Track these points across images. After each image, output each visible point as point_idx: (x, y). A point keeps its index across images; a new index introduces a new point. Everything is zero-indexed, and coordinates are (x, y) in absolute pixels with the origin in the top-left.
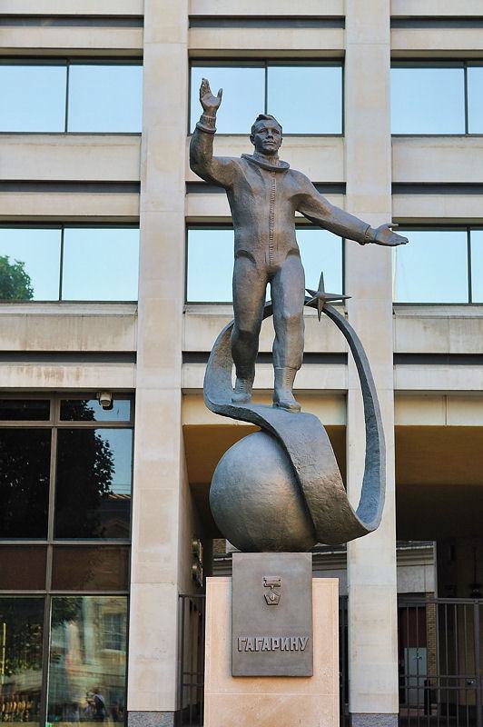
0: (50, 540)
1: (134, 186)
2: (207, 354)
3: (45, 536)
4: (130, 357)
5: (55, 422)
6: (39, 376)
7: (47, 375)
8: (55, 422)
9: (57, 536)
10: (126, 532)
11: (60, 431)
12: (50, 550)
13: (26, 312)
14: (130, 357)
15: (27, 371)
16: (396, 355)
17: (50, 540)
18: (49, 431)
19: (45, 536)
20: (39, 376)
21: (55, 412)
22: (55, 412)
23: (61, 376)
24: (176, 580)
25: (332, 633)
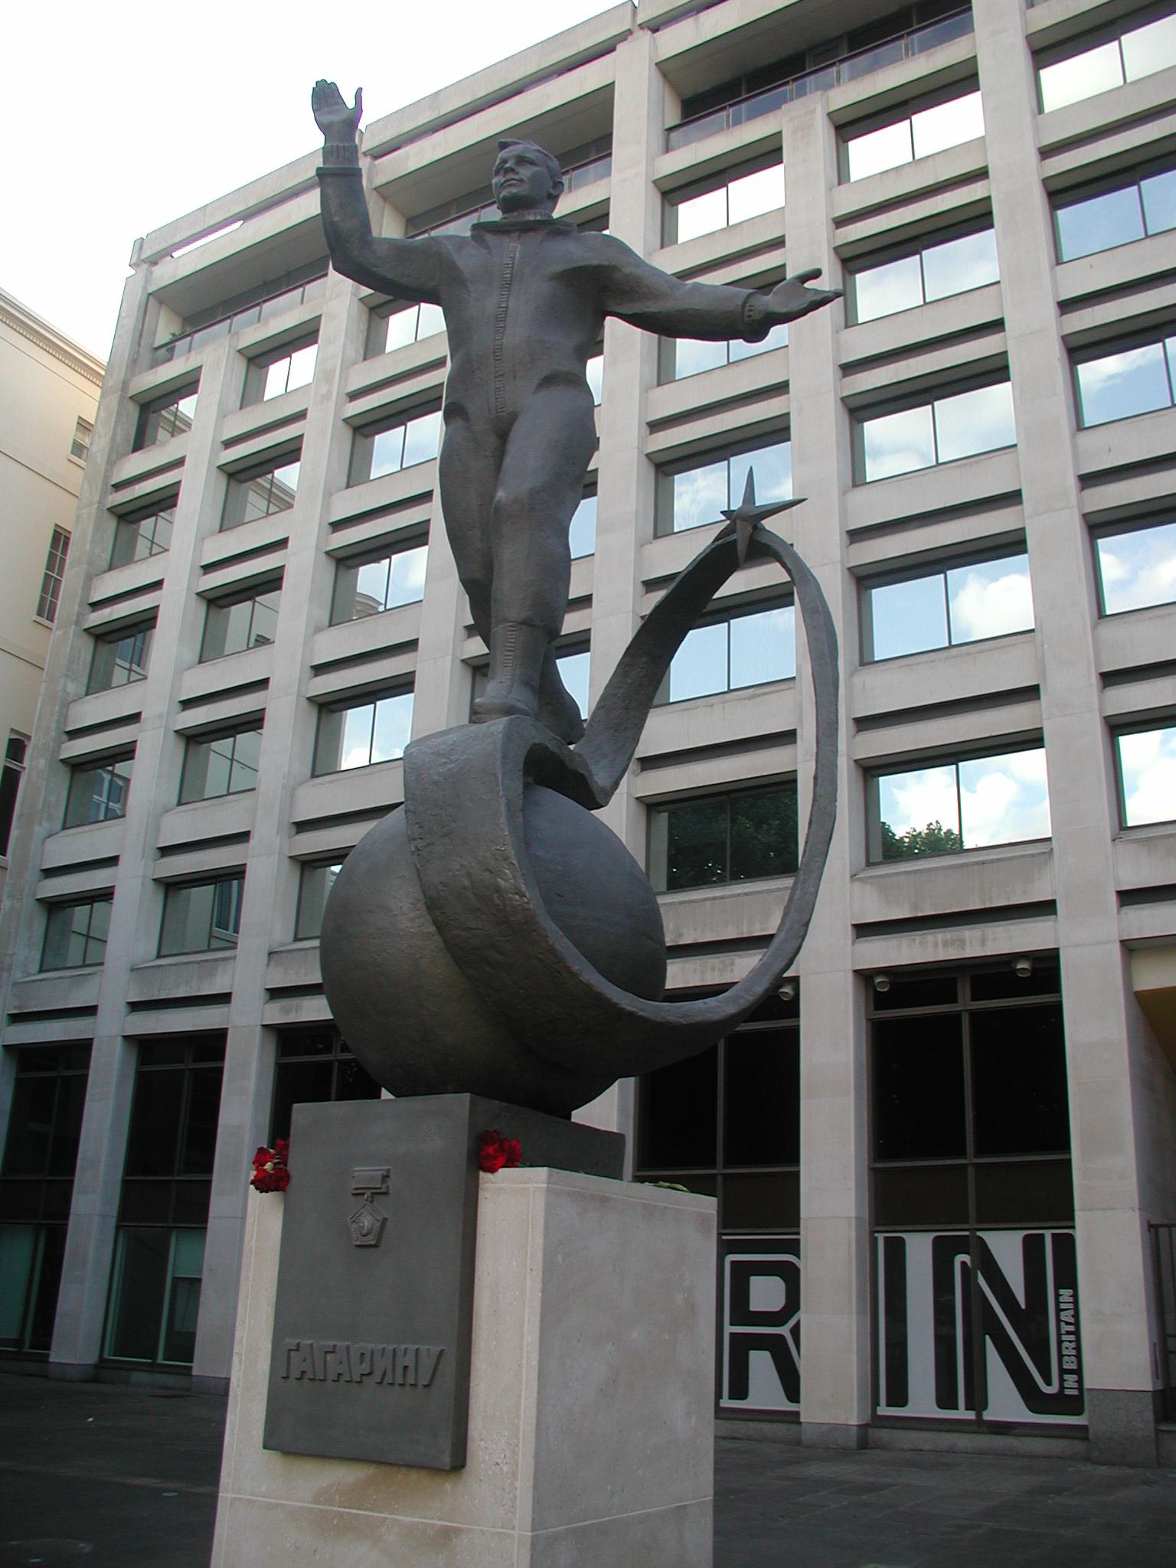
0: (971, 1159)
1: (1031, 693)
2: (769, 938)
3: (962, 1153)
4: (1047, 908)
5: (965, 1003)
6: (936, 945)
7: (945, 944)
8: (965, 1003)
9: (980, 1151)
10: (1066, 1146)
11: (974, 1015)
12: (971, 1171)
13: (710, 895)
14: (1047, 908)
15: (921, 943)
16: (1120, 893)
17: (971, 1159)
18: (956, 1017)
19: (962, 1153)
20: (936, 945)
21: (964, 991)
22: (964, 991)
23: (962, 943)
24: (1136, 1203)
25: (522, 1337)
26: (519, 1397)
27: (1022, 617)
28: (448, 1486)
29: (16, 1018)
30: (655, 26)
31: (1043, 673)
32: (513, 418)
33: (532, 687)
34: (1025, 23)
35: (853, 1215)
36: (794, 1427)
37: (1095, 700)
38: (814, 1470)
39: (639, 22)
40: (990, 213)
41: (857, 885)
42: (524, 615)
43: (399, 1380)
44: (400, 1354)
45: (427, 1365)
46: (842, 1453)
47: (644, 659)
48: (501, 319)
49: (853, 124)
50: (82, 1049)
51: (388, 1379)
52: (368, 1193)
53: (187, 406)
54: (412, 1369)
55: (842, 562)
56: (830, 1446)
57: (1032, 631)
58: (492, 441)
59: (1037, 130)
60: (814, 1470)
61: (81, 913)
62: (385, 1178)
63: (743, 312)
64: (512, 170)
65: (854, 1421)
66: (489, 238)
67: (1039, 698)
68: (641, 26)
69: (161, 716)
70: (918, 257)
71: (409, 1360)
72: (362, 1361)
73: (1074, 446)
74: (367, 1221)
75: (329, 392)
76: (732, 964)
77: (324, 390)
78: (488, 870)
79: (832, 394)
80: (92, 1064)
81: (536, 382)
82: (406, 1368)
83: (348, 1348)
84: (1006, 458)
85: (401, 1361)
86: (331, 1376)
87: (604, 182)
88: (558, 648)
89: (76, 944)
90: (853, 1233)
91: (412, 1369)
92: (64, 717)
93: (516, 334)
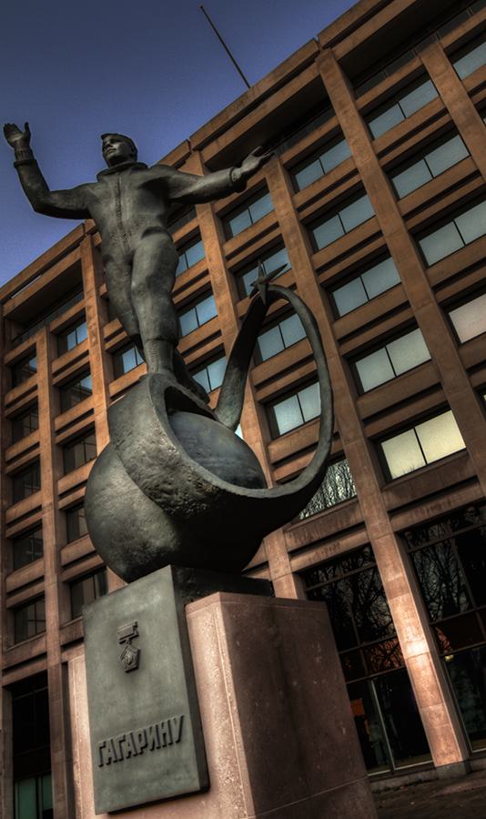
1: (437, 387)
20: (428, 511)
25: (225, 695)
26: (231, 731)
27: (424, 355)
28: (203, 802)
29: (7, 671)
30: (200, 148)
31: (440, 376)
32: (133, 253)
33: (169, 369)
34: (356, 106)
35: (428, 651)
36: (433, 772)
37: (468, 382)
38: (449, 790)
39: (192, 147)
40: (363, 187)
41: (384, 493)
42: (157, 335)
43: (162, 743)
44: (160, 727)
45: (175, 729)
46: (460, 779)
47: (236, 369)
48: (119, 211)
49: (292, 169)
50: (44, 674)
51: (157, 745)
52: (127, 639)
53: (33, 363)
54: (168, 734)
55: (339, 354)
56: (453, 776)
57: (430, 360)
58: (125, 268)
59: (373, 149)
60: (449, 790)
61: (30, 610)
62: (136, 627)
63: (231, 178)
64: (109, 146)
65: (461, 759)
66: (106, 178)
67: (442, 388)
68: (194, 150)
69: (51, 504)
70: (359, 279)
71: (166, 729)
72: (140, 740)
73: (426, 275)
74: (129, 655)
75: (96, 340)
76: (338, 544)
77: (94, 340)
78: (153, 442)
79: (315, 284)
80: (49, 682)
81: (141, 234)
82: (164, 735)
83: (131, 734)
84: (399, 288)
85: (161, 732)
86: (126, 755)
87: (195, 220)
88: (190, 370)
89: (31, 626)
90: (431, 660)
91: (168, 734)
92: (4, 516)
93: (127, 215)
